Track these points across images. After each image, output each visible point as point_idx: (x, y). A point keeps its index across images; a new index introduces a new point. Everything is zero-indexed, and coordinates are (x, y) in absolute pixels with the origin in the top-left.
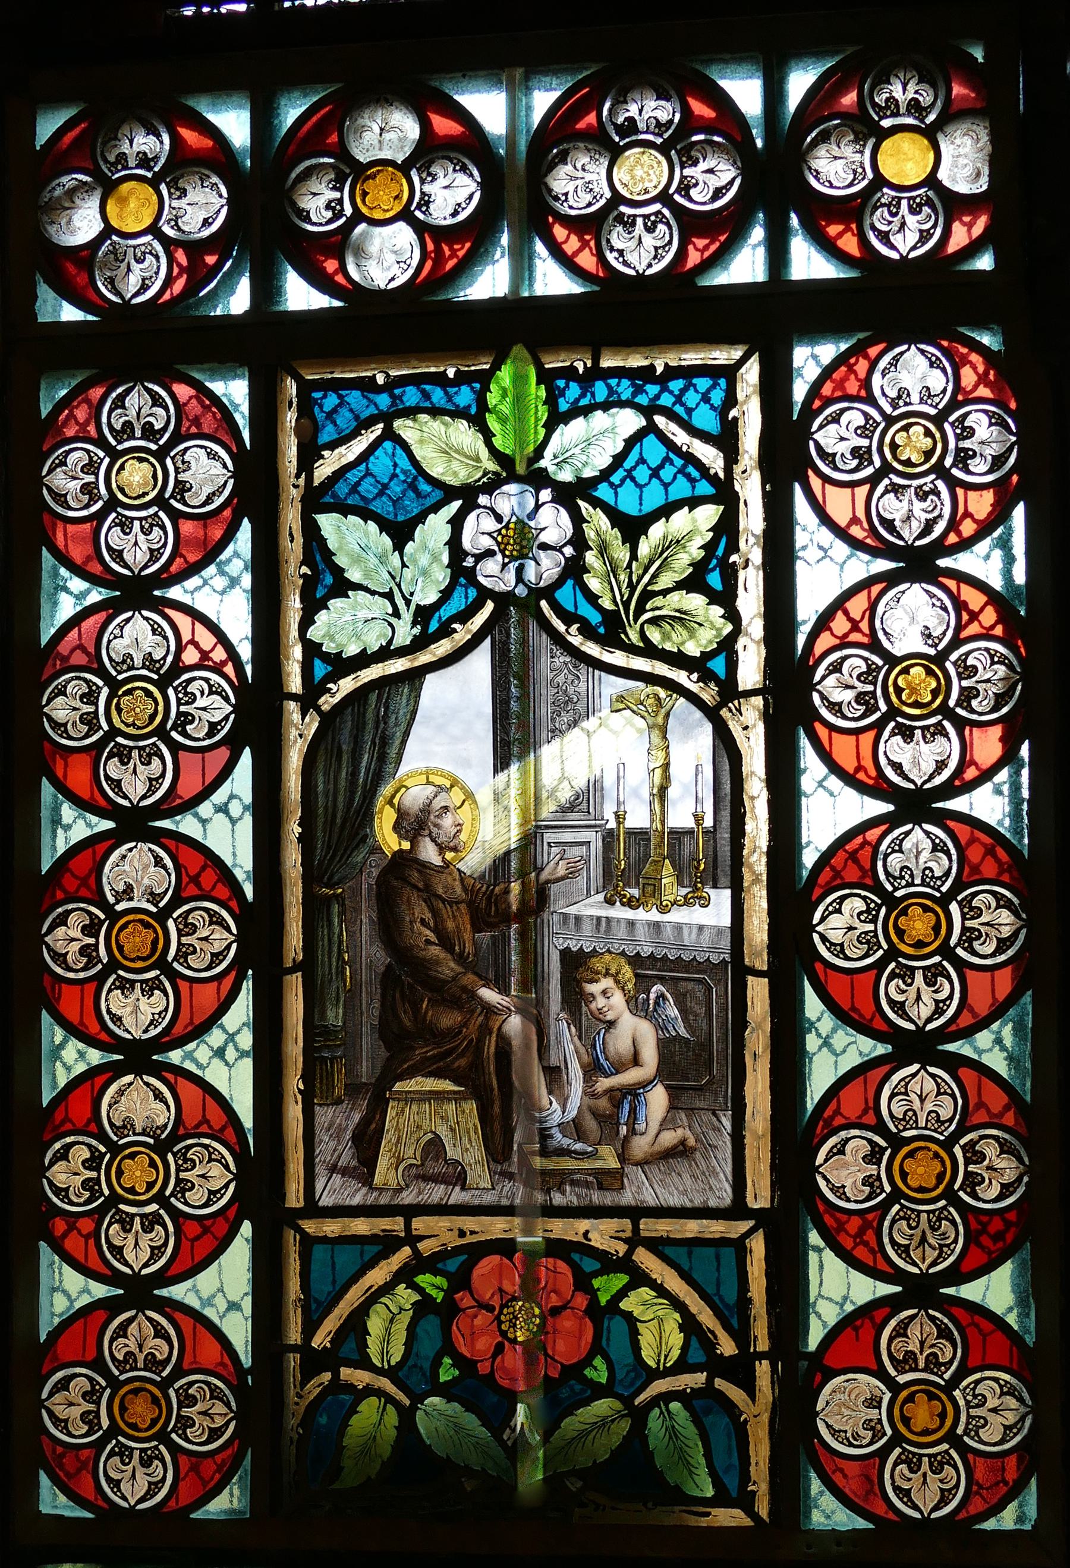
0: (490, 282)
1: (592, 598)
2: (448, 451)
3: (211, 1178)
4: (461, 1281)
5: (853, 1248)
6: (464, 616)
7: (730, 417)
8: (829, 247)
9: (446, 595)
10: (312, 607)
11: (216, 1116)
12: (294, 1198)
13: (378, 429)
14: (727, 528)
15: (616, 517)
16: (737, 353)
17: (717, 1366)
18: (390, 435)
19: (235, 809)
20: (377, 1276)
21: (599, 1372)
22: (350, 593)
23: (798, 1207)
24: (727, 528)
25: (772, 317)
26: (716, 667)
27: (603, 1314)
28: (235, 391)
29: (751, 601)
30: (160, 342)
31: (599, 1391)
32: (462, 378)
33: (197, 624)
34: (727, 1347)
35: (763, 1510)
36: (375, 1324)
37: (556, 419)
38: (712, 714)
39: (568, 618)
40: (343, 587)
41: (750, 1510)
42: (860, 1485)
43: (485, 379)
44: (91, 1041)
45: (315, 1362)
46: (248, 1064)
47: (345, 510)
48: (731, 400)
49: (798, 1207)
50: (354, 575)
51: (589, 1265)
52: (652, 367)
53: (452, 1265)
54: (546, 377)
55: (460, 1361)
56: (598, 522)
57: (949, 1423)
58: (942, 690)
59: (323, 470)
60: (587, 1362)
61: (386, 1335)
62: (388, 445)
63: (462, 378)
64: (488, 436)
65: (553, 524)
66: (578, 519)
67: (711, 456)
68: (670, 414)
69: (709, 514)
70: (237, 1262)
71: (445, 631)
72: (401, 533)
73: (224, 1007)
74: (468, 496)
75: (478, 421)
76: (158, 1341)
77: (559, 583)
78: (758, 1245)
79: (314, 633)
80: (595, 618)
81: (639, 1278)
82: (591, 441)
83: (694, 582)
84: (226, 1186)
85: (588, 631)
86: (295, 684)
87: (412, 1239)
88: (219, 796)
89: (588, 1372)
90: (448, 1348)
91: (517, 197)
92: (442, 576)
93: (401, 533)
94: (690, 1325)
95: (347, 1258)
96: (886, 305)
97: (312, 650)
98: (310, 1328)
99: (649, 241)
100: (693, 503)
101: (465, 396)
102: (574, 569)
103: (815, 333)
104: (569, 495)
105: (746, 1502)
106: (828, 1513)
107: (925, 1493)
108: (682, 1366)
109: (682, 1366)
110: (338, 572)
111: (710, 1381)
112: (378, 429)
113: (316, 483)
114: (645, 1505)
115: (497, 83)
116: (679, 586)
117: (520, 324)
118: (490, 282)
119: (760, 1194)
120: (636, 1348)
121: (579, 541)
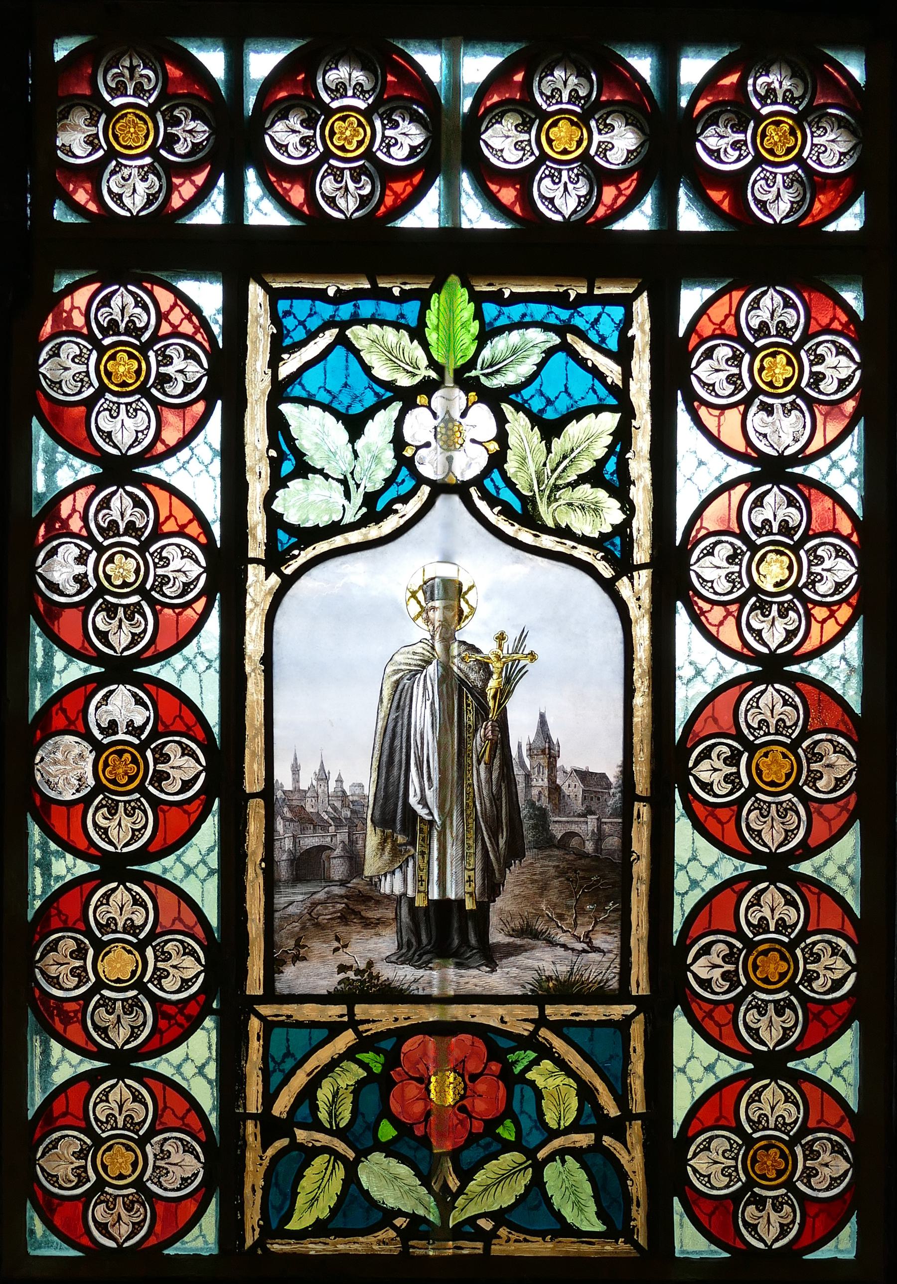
0: (425, 215)
1: (511, 485)
2: (392, 357)
3: (183, 971)
4: (393, 1059)
5: (703, 890)
6: (405, 499)
7: (630, 334)
8: (710, 208)
9: (389, 481)
10: (278, 482)
11: (190, 918)
12: (254, 985)
13: (329, 336)
14: (622, 436)
15: (536, 419)
16: (642, 1240)
17: (606, 1126)
18: (342, 340)
19: (202, 664)
20: (323, 1056)
21: (507, 1132)
22: (310, 475)
23: (670, 988)
24: (622, 436)
25: (662, 263)
26: (615, 546)
27: (513, 1080)
28: (208, 295)
29: (641, 494)
30: (152, 248)
31: (507, 1147)
32: (407, 295)
33: (173, 498)
34: (613, 1111)
35: (642, 1240)
36: (324, 1094)
37: (485, 336)
38: (609, 586)
39: (493, 501)
40: (304, 469)
41: (630, 1240)
42: (716, 1216)
43: (424, 298)
44: (78, 854)
45: (272, 1128)
46: (214, 880)
47: (307, 401)
48: (628, 321)
49: (670, 988)
50: (315, 459)
51: (504, 1043)
52: (566, 294)
53: (387, 1044)
54: (477, 298)
55: (395, 1122)
56: (519, 425)
57: (751, 958)
58: (779, 549)
59: (289, 366)
60: (498, 1121)
61: (337, 1095)
62: (340, 351)
63: (407, 295)
64: (425, 345)
65: (482, 422)
66: (501, 420)
67: (612, 370)
68: (582, 335)
69: (610, 421)
70: (202, 1044)
71: (389, 511)
72: (355, 426)
73: (195, 828)
74: (408, 398)
75: (418, 333)
76: (136, 1105)
77: (486, 472)
78: (637, 1029)
79: (277, 506)
80: (517, 505)
81: (545, 1052)
82: (519, 352)
83: (594, 477)
84: (197, 976)
85: (507, 512)
86: (256, 550)
87: (353, 1023)
88: (190, 650)
89: (500, 1130)
90: (386, 1113)
91: (453, 147)
92: (389, 462)
93: (355, 426)
94: (586, 1093)
95: (299, 1038)
96: (745, 254)
97: (275, 521)
98: (269, 1098)
99: (831, 360)
100: (597, 409)
101: (411, 309)
102: (497, 461)
103: (699, 277)
104: (494, 399)
105: (628, 1234)
106: (689, 1241)
107: (769, 1228)
108: (576, 1127)
109: (576, 1127)
110: (299, 455)
111: (598, 1140)
112: (329, 336)
113: (280, 378)
114: (544, 1239)
115: (439, 47)
116: (582, 479)
117: (451, 255)
118: (425, 215)
119: (640, 981)
120: (541, 1114)
121: (502, 437)
